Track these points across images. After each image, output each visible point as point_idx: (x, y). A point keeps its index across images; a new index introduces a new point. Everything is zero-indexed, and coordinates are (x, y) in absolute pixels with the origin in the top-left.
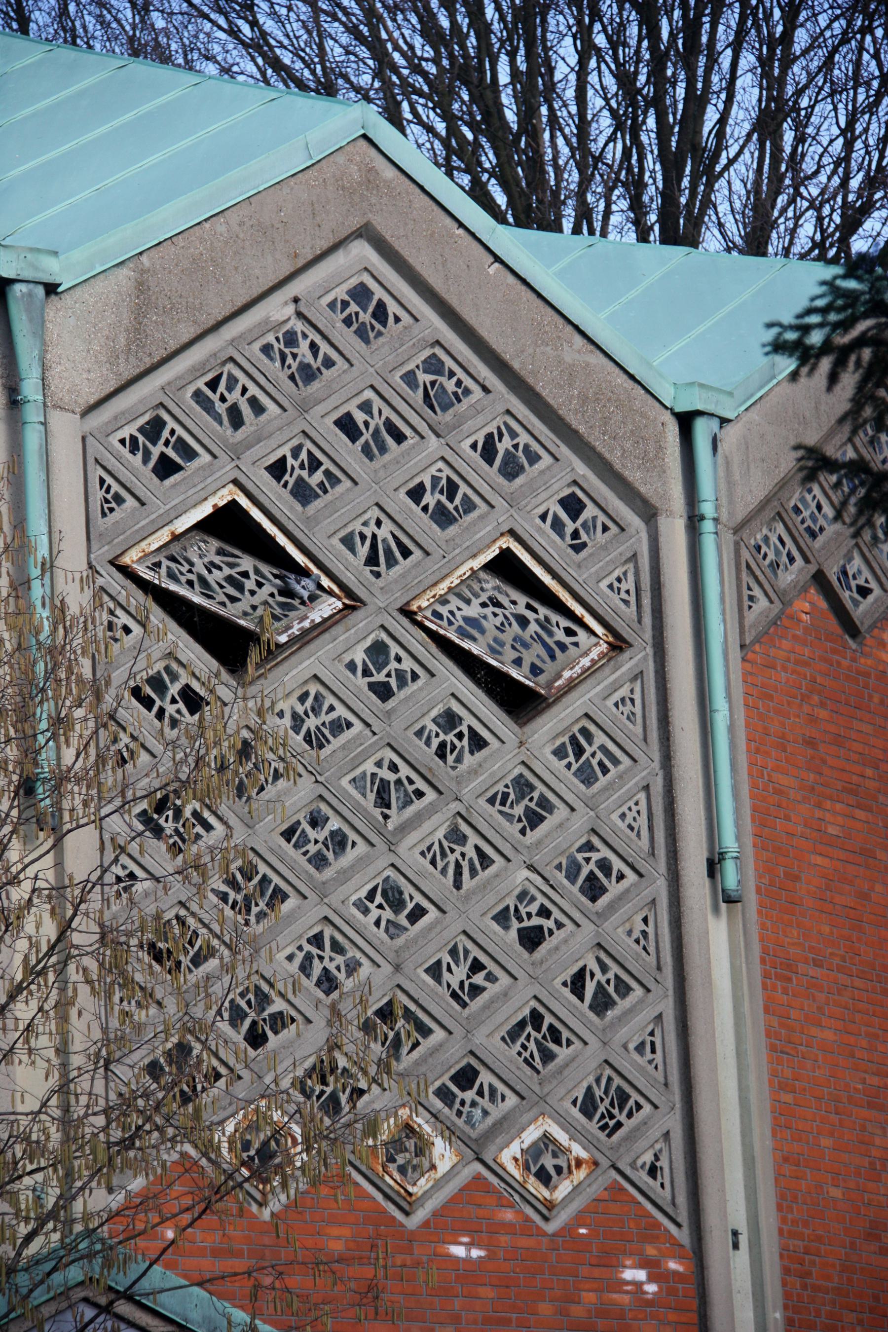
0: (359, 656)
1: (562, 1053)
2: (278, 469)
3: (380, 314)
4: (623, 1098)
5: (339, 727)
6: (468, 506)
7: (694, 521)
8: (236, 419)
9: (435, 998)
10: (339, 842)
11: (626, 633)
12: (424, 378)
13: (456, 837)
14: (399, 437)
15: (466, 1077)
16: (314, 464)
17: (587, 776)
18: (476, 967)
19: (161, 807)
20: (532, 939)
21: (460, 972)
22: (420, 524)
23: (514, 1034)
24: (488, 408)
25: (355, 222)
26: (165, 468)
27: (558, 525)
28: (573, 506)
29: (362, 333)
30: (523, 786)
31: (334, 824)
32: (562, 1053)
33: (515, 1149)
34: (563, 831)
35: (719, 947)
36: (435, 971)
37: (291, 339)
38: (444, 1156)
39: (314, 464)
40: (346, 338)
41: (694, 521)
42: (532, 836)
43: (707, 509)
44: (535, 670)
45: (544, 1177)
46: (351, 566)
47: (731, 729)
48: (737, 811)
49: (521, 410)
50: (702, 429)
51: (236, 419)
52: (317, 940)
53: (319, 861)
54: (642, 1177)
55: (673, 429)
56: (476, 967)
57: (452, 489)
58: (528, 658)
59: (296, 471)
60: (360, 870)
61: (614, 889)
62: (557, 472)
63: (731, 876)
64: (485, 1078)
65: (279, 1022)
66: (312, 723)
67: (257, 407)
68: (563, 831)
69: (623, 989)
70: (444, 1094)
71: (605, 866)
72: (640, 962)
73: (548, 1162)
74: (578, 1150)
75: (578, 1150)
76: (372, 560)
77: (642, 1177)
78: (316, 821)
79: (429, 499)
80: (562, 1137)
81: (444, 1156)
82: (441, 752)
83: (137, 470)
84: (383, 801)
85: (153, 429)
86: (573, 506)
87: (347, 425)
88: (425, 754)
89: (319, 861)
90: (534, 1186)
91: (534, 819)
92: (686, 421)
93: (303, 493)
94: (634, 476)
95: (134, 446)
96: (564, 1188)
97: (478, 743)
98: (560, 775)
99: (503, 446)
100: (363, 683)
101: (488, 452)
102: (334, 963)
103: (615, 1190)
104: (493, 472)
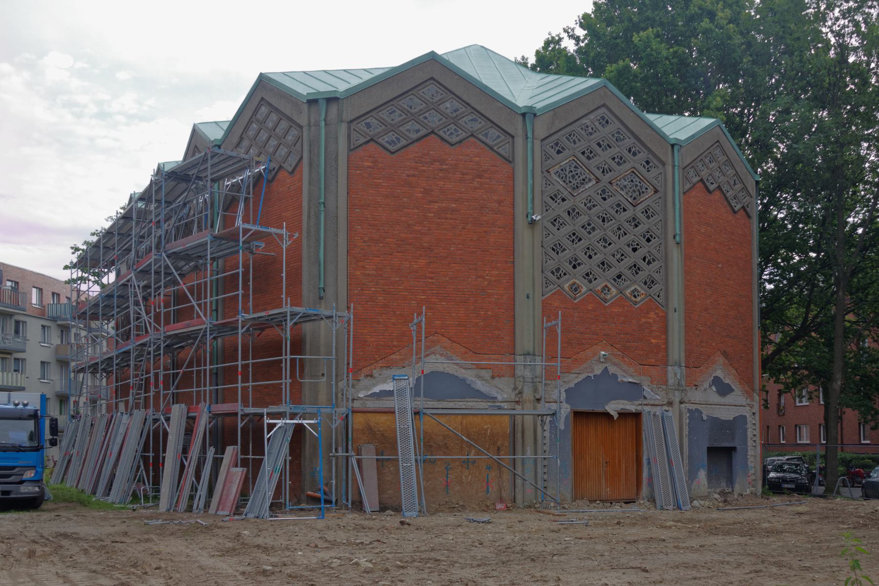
0: (600, 192)
1: (640, 273)
2: (583, 153)
3: (607, 122)
4: (653, 282)
5: (594, 206)
6: (625, 162)
7: (674, 166)
8: (575, 142)
9: (613, 261)
10: (594, 229)
11: (659, 188)
12: (616, 135)
13: (619, 229)
14: (610, 147)
15: (619, 277)
16: (591, 152)
17: (648, 217)
18: (622, 255)
19: (555, 220)
20: (635, 250)
21: (619, 256)
22: (613, 164)
23: (630, 268)
24: (629, 141)
25: (602, 103)
26: (559, 152)
27: (644, 167)
28: (648, 162)
29: (603, 126)
30: (634, 219)
31: (593, 225)
32: (640, 273)
33: (629, 291)
34: (641, 228)
35: (676, 256)
36: (613, 255)
37: (587, 127)
38: (614, 291)
39: (591, 152)
40: (600, 127)
41: (674, 166)
42: (636, 229)
43: (676, 164)
44: (635, 199)
45: (635, 296)
46: (599, 173)
47: (680, 208)
48: (680, 222)
49: (621, 127)
50: (676, 148)
51: (575, 142)
52: (588, 249)
53: (589, 233)
54: (656, 297)
55: (670, 147)
56: (622, 255)
57: (621, 158)
58: (634, 195)
59: (587, 153)
60: (598, 234)
61: (653, 240)
62: (643, 156)
63: (678, 238)
64: (623, 277)
65: (579, 264)
66: (589, 205)
67: (579, 141)
68: (641, 228)
69: (654, 260)
70: (614, 280)
71: (651, 236)
72: (658, 232)
73: (636, 294)
74: (643, 292)
75: (643, 292)
76: (603, 172)
77: (656, 297)
78: (589, 225)
79: (616, 160)
80: (639, 289)
81: (614, 291)
82: (617, 212)
83: (553, 152)
84: (603, 221)
85: (557, 144)
86: (648, 162)
87: (599, 145)
88: (613, 212)
89: (589, 233)
90: (633, 298)
91: (636, 226)
92: (673, 146)
93: (589, 158)
94: (661, 156)
95: (552, 147)
96: (639, 299)
97: (625, 210)
98: (642, 217)
99: (633, 150)
100: (600, 197)
101: (630, 151)
102: (592, 253)
103: (650, 300)
104: (630, 155)
